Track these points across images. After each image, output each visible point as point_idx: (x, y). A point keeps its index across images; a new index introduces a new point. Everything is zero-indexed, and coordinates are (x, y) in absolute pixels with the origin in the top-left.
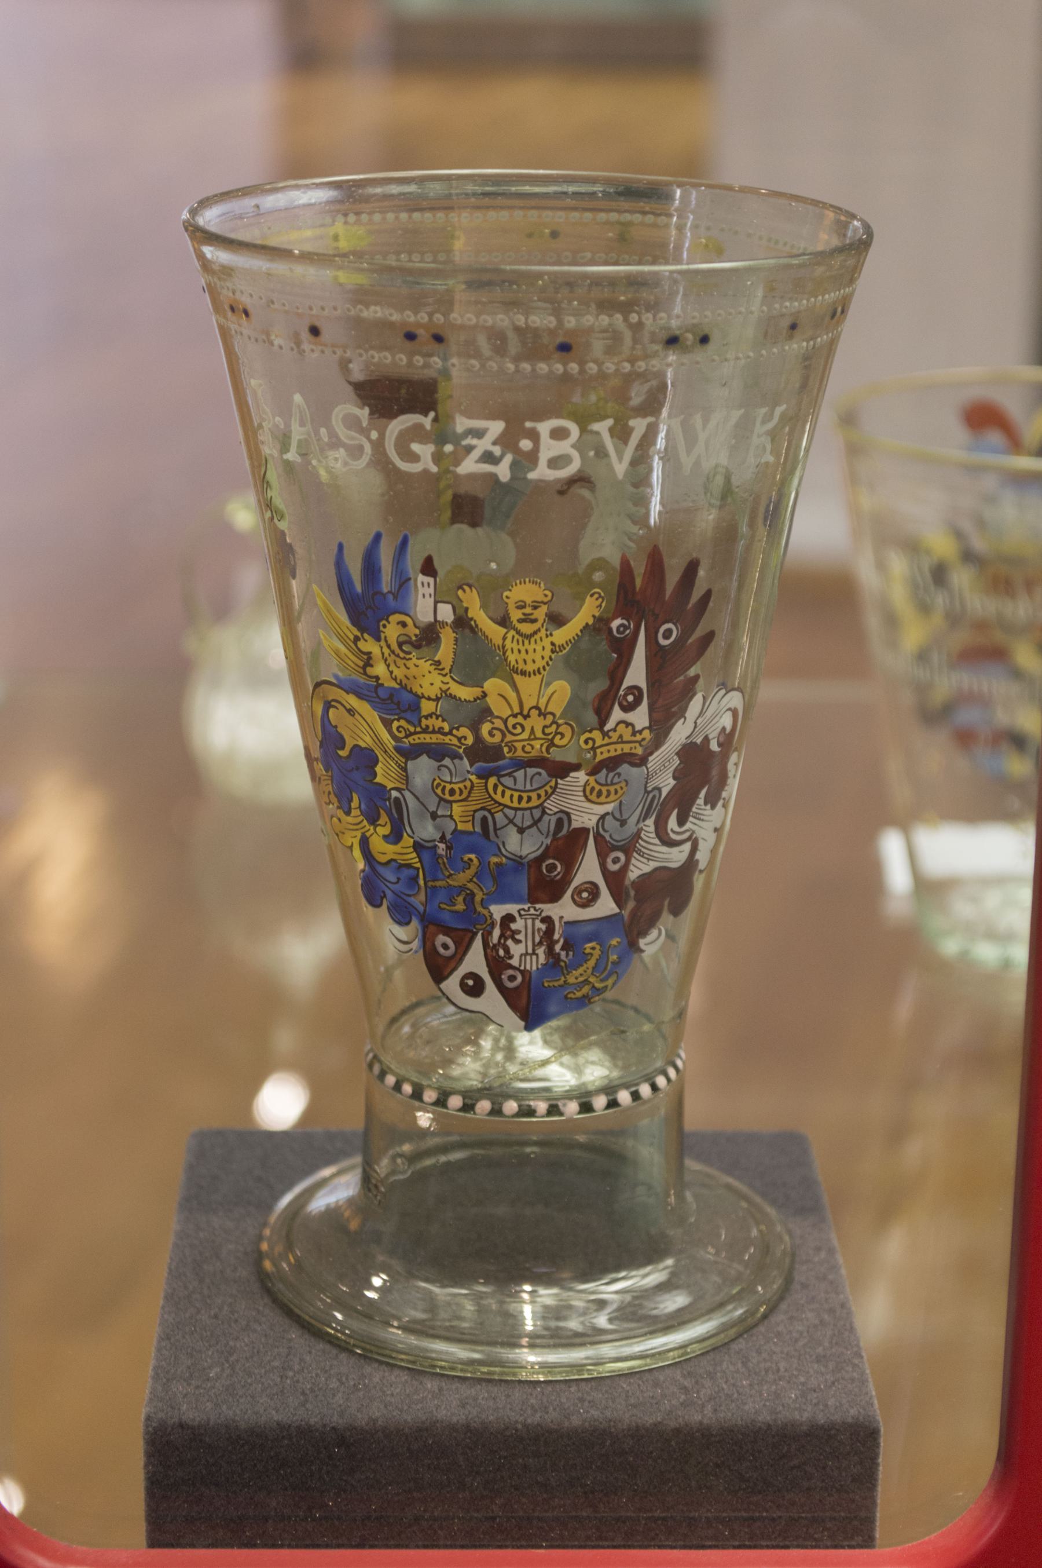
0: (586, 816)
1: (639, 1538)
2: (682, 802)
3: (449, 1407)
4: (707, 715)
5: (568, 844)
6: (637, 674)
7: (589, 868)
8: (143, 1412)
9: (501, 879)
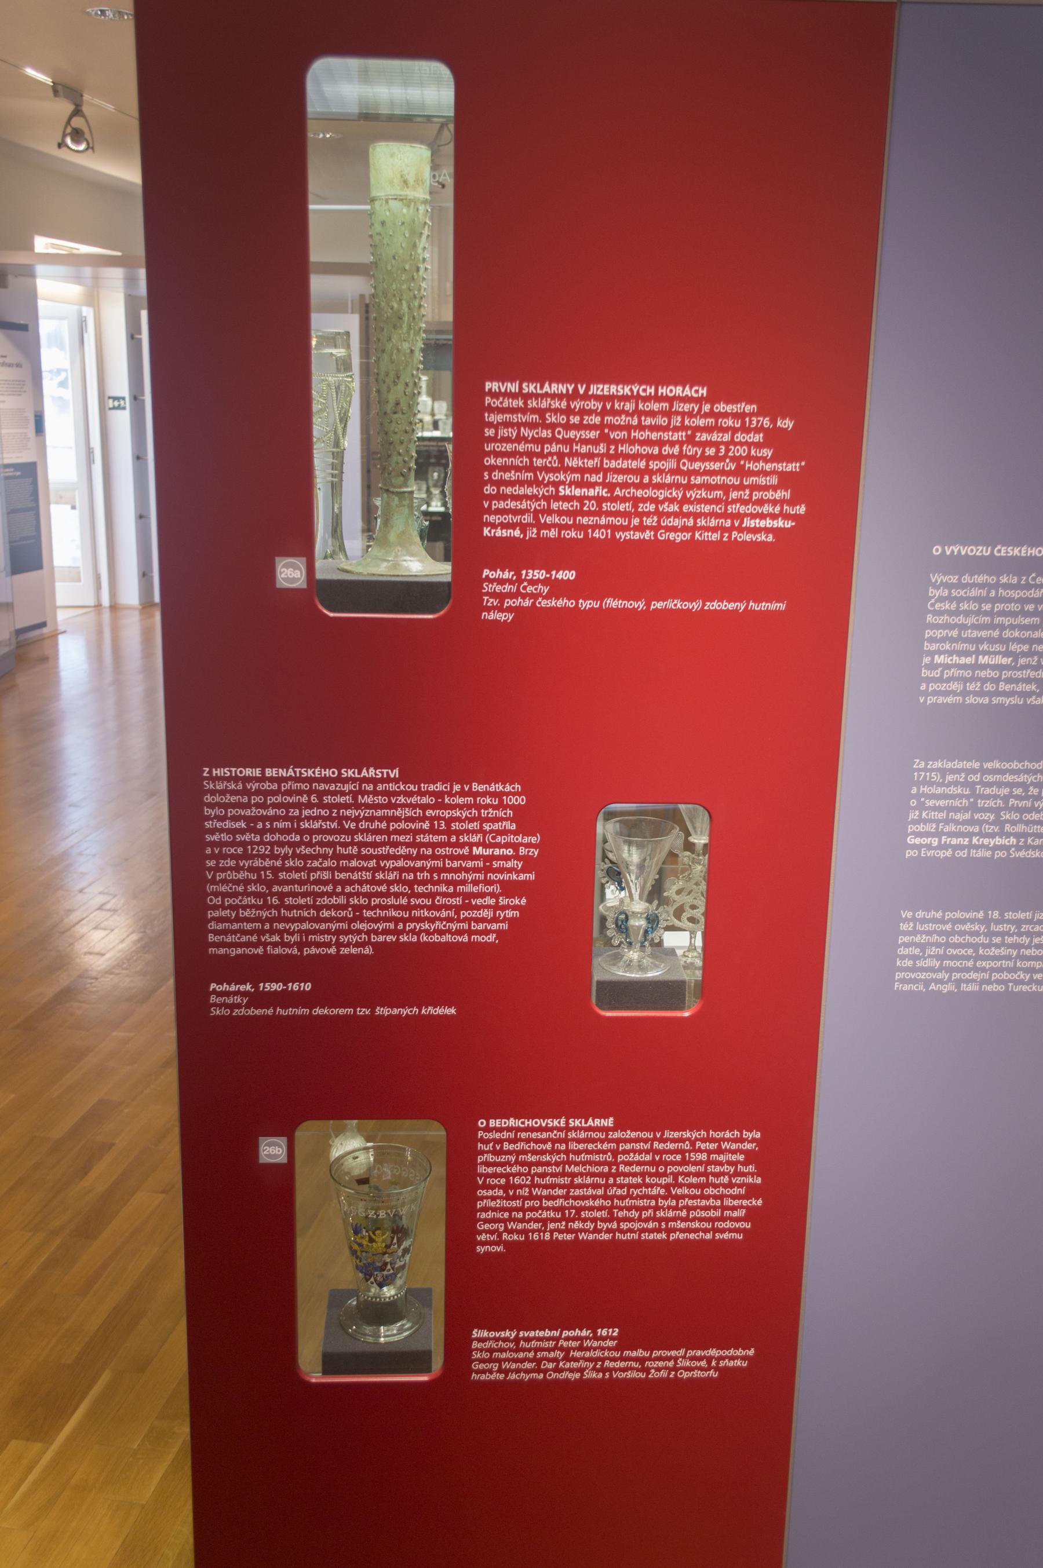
0: (388, 1260)
1: (634, 955)
2: (403, 1256)
3: (368, 1349)
4: (406, 1244)
5: (386, 1264)
6: (395, 1241)
7: (389, 1267)
8: (321, 1349)
9: (376, 1269)
